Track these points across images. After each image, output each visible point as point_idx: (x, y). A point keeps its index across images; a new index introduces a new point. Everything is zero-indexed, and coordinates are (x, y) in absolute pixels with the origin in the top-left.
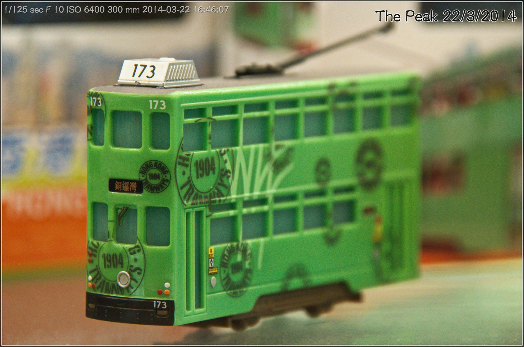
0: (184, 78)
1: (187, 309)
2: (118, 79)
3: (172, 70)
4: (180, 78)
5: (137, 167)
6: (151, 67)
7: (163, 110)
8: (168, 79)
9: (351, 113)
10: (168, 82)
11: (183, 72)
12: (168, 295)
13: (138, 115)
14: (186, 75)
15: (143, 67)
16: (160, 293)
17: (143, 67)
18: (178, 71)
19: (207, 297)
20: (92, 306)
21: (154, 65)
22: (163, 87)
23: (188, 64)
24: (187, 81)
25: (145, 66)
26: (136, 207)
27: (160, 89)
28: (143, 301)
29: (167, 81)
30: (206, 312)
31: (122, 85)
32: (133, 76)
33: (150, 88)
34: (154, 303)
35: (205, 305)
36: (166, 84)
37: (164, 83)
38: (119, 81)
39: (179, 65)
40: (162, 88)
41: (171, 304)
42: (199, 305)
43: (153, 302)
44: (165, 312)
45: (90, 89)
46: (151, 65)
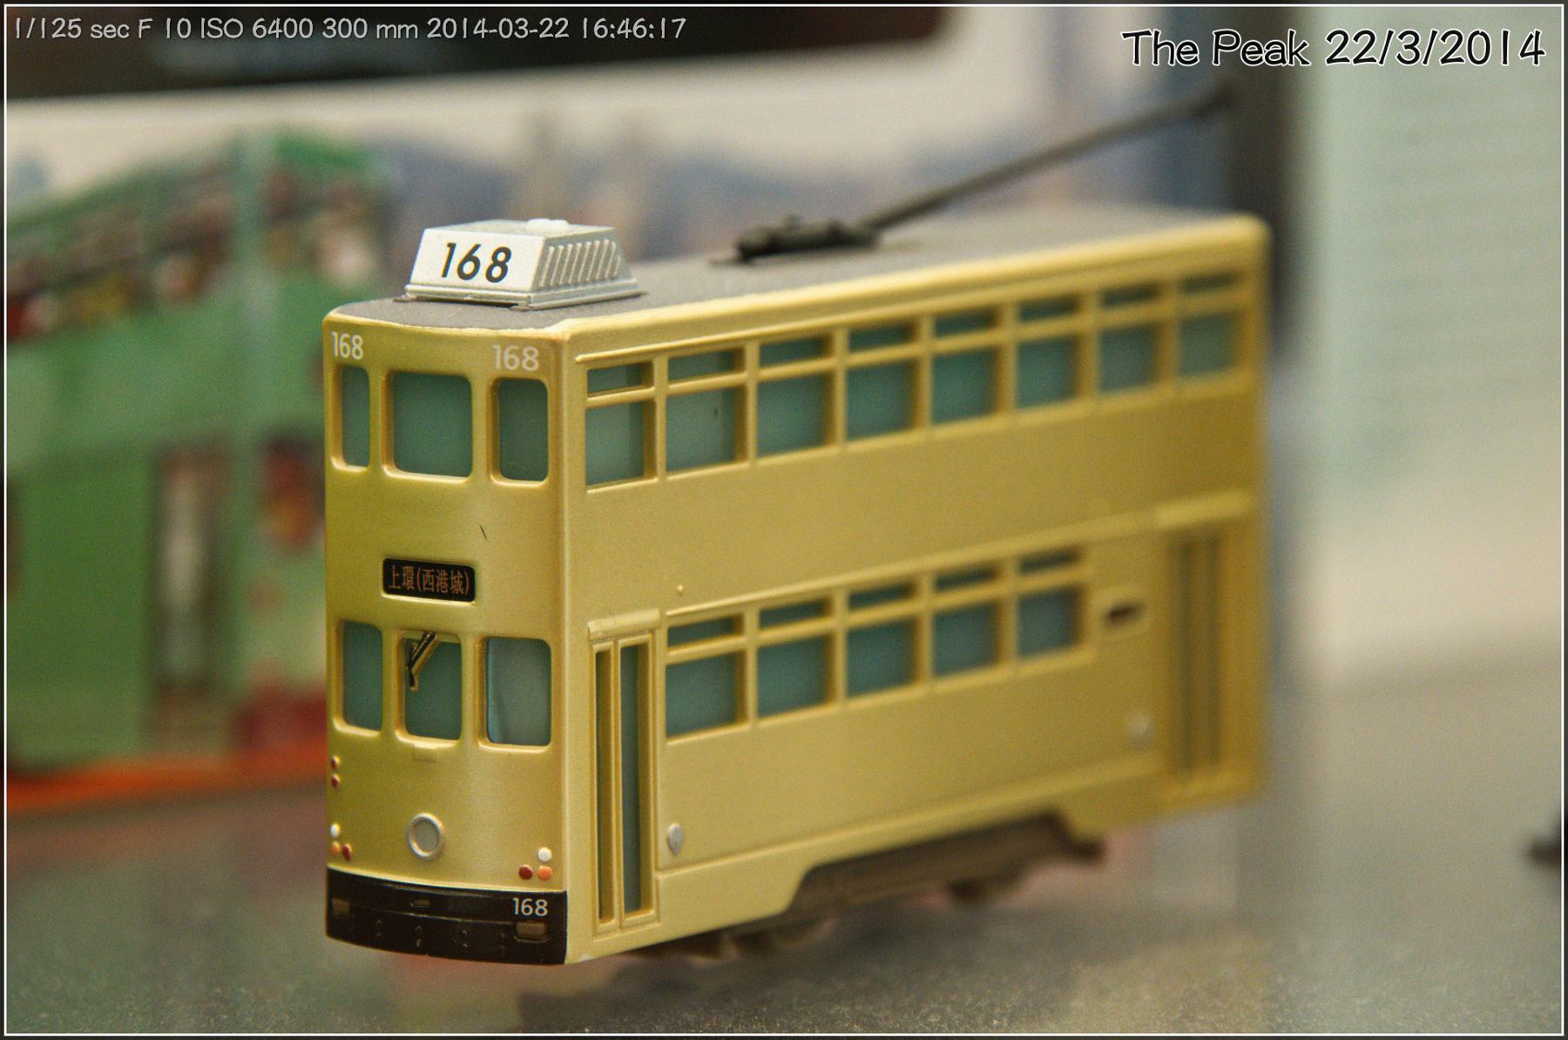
1: (600, 917)
2: (407, 280)
4: (551, 284)
7: (535, 372)
8: (542, 285)
10: (543, 294)
12: (545, 878)
13: (458, 385)
16: (525, 874)
23: (599, 240)
26: (459, 640)
27: (521, 314)
28: (481, 896)
30: (658, 918)
32: (445, 274)
37: (530, 294)
41: (558, 902)
42: (637, 898)
43: (512, 900)
45: (328, 311)
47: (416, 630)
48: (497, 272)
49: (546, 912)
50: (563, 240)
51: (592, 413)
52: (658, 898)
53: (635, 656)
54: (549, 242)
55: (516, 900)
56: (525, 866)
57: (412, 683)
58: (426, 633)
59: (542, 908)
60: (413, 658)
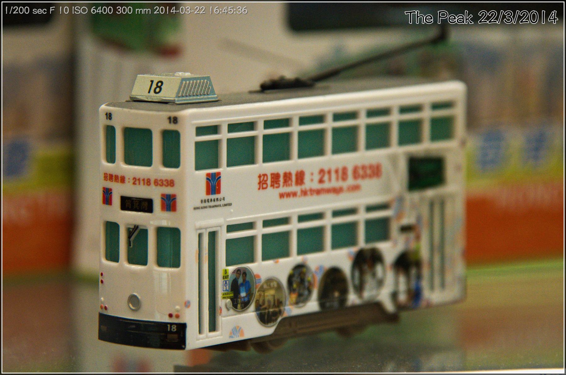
0: (184, 95)
3: (185, 86)
5: (107, 181)
9: (416, 125)
10: (180, 99)
12: (177, 316)
19: (221, 320)
22: (174, 104)
23: (184, 81)
24: (195, 98)
29: (179, 97)
30: (221, 335)
32: (149, 92)
34: (168, 326)
35: (220, 328)
39: (200, 80)
41: (182, 327)
42: (213, 327)
44: (176, 336)
47: (131, 225)
48: (158, 90)
49: (175, 330)
50: (189, 79)
51: (198, 144)
52: (222, 327)
53: (213, 236)
54: (183, 79)
55: (169, 325)
56: (135, 294)
57: (130, 245)
58: (135, 226)
59: (174, 328)
60: (131, 235)
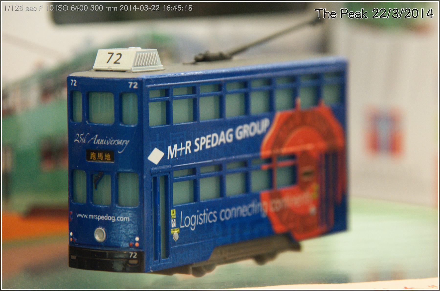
2: (93, 65)
6: (117, 54)
10: (136, 68)
11: (147, 59)
14: (151, 62)
15: (111, 55)
17: (111, 55)
18: (144, 58)
20: (74, 257)
21: (122, 54)
25: (112, 54)
29: (135, 66)
31: (97, 70)
33: (144, 73)
36: (134, 69)
38: (94, 67)
40: (130, 73)
46: (117, 53)
